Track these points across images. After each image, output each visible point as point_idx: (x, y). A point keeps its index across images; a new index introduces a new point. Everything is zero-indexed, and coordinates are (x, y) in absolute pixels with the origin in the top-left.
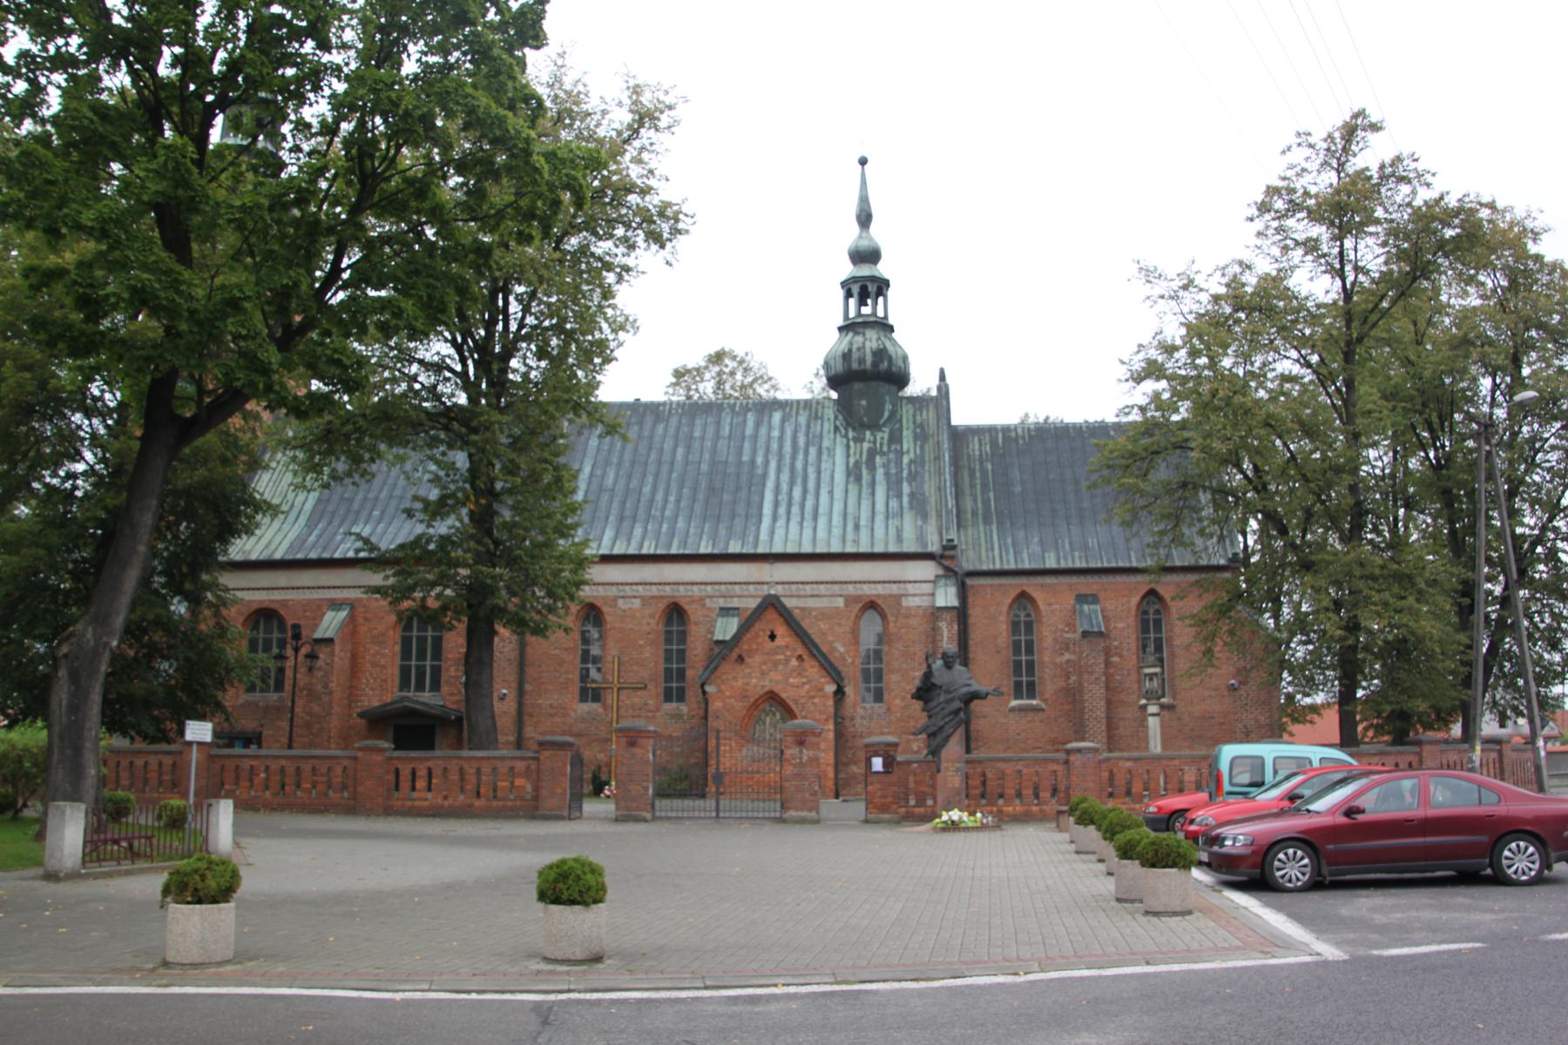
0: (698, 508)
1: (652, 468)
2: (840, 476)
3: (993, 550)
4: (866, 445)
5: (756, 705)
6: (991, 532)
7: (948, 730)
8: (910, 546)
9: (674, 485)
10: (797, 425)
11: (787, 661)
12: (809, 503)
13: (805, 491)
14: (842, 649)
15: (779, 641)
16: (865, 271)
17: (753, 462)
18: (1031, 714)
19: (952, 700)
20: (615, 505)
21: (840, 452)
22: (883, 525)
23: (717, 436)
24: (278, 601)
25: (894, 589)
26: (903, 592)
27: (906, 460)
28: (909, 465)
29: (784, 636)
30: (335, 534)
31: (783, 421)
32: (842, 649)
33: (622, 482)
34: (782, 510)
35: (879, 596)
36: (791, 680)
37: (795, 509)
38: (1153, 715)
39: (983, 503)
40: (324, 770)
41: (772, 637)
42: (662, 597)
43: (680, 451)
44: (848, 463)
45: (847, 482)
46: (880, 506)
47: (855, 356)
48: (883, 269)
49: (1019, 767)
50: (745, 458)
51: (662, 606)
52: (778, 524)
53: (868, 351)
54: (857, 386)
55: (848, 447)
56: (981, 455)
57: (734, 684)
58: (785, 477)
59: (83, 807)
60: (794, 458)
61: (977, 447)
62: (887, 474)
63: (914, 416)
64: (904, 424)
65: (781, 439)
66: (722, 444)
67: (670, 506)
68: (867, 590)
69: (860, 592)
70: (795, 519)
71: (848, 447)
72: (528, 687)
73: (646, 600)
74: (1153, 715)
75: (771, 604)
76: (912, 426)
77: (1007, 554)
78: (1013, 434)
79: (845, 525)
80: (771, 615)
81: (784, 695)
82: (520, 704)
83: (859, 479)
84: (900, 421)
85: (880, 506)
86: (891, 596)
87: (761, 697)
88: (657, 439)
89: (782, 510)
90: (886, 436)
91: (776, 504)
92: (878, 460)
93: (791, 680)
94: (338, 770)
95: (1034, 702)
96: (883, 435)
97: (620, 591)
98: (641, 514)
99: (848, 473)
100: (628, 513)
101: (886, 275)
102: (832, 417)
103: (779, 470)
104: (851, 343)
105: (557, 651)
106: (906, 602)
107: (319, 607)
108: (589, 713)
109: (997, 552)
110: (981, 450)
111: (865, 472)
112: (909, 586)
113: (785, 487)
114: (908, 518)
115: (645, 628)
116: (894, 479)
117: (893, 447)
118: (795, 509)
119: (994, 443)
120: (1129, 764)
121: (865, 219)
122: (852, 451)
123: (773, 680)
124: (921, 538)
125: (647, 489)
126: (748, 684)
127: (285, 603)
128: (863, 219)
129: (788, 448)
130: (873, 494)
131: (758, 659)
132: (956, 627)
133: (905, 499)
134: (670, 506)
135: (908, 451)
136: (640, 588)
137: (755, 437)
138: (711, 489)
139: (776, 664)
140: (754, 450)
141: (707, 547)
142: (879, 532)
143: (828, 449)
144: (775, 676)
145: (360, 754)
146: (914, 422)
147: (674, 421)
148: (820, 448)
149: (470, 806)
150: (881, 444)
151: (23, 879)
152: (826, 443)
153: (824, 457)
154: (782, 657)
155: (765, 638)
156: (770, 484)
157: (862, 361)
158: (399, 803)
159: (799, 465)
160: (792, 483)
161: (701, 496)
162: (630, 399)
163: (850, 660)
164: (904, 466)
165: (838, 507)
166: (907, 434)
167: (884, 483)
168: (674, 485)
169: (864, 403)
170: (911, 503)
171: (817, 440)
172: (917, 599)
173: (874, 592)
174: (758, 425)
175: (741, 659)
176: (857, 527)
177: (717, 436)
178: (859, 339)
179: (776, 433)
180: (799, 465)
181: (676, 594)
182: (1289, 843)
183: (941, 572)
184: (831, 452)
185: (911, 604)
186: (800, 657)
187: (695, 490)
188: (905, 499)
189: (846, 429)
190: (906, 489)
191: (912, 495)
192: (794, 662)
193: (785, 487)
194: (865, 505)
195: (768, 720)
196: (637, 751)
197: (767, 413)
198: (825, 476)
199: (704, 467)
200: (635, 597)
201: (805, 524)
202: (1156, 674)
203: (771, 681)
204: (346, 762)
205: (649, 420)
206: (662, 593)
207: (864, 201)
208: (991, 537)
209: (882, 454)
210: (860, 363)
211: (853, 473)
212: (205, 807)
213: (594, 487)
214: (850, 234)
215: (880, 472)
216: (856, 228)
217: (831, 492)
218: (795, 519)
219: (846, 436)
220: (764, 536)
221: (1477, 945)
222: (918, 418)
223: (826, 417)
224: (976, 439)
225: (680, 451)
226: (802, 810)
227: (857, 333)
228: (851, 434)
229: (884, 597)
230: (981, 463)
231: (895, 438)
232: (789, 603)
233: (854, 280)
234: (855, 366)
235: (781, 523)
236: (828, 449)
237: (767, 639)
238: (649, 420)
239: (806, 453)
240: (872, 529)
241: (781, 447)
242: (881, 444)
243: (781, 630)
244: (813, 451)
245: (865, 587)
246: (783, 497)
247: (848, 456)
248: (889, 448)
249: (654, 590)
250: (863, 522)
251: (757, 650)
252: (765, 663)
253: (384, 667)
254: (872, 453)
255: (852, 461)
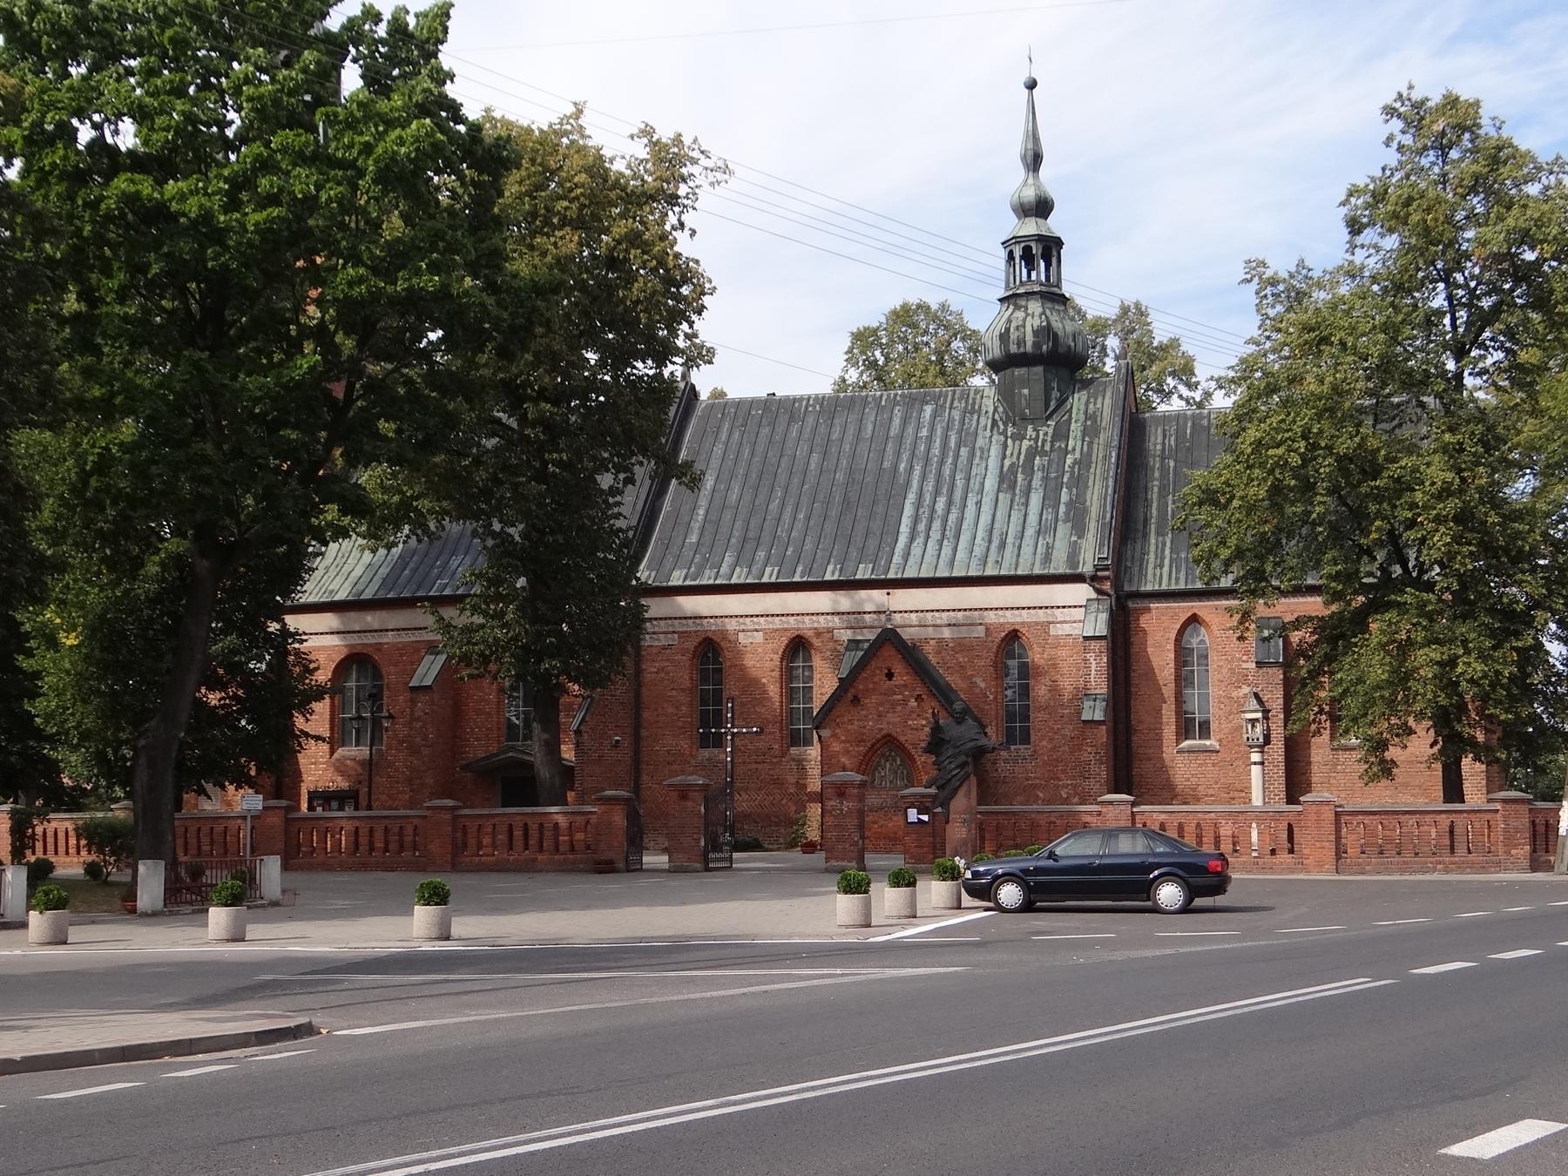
0: (829, 527)
1: (782, 478)
2: (991, 483)
3: (1161, 567)
4: (1026, 443)
5: (872, 750)
6: (1164, 544)
7: (955, 783)
8: (1059, 566)
9: (805, 500)
10: (950, 420)
11: (905, 701)
12: (952, 517)
13: (950, 503)
14: (983, 685)
15: (897, 680)
16: (1031, 227)
17: (895, 468)
18: (1202, 756)
19: (959, 754)
20: (738, 524)
21: (995, 451)
22: (1032, 542)
23: (858, 437)
24: (371, 645)
25: (1041, 616)
26: (1051, 619)
27: (1069, 461)
28: (1072, 467)
29: (902, 676)
30: (432, 566)
31: (935, 415)
32: (983, 685)
33: (747, 497)
34: (921, 527)
35: (1023, 623)
36: (910, 722)
37: (937, 525)
38: (1255, 763)
39: (1158, 509)
40: (396, 830)
41: (890, 676)
42: (786, 630)
43: (815, 457)
44: (1002, 466)
45: (999, 491)
46: (1033, 518)
47: (1014, 336)
48: (1055, 224)
49: (1053, 819)
50: (886, 464)
51: (785, 641)
52: (915, 544)
53: (1029, 329)
54: (1018, 372)
55: (1005, 446)
56: (1163, 450)
57: (850, 727)
58: (929, 487)
59: (163, 863)
60: (942, 462)
61: (1160, 439)
62: (1045, 479)
63: (1087, 404)
64: (1074, 415)
65: (930, 439)
66: (863, 447)
67: (799, 525)
68: (1011, 618)
69: (1002, 620)
70: (935, 535)
71: (1005, 446)
72: (644, 733)
73: (769, 634)
74: (1255, 763)
75: (889, 638)
76: (1082, 417)
77: (1178, 572)
78: (1205, 422)
79: (990, 541)
80: (888, 651)
81: (902, 739)
82: (637, 752)
83: (1013, 486)
84: (1070, 410)
85: (1033, 518)
86: (1037, 623)
87: (878, 741)
88: (790, 444)
89: (921, 527)
90: (1051, 431)
91: (916, 520)
92: (1037, 461)
93: (910, 722)
94: (409, 830)
95: (1208, 743)
96: (1049, 429)
97: (740, 624)
98: (766, 537)
99: (1002, 478)
100: (751, 534)
101: (1057, 232)
102: (991, 409)
103: (924, 477)
104: (1009, 321)
105: (674, 693)
106: (1058, 630)
107: (417, 650)
108: (709, 759)
109: (1166, 568)
110: (1164, 444)
111: (1020, 477)
112: (1057, 612)
113: (928, 498)
114: (1063, 530)
115: (768, 664)
116: (1053, 484)
117: (1057, 444)
118: (937, 525)
119: (1180, 434)
120: (1163, 816)
121: (1034, 161)
122: (1008, 453)
123: (891, 723)
124: (1073, 558)
125: (774, 506)
126: (865, 727)
127: (378, 647)
128: (1030, 159)
129: (936, 451)
130: (1026, 504)
131: (874, 699)
132: (1105, 659)
133: (1062, 509)
134: (799, 525)
135: (1074, 449)
136: (762, 620)
137: (901, 436)
138: (846, 500)
139: (894, 705)
140: (898, 455)
141: (833, 573)
142: (1027, 550)
143: (982, 449)
144: (893, 718)
145: (428, 813)
146: (1086, 412)
147: (810, 420)
148: (973, 448)
149: (535, 860)
150: (1044, 441)
151: (208, 1020)
152: (980, 442)
153: (977, 461)
154: (900, 697)
155: (880, 677)
156: (911, 497)
157: (1021, 342)
158: (468, 860)
159: (947, 471)
160: (937, 493)
161: (833, 513)
162: (761, 393)
163: (991, 697)
164: (1067, 469)
165: (985, 519)
166: (1076, 428)
167: (1041, 490)
168: (805, 500)
169: (1026, 391)
170: (1067, 513)
171: (970, 438)
172: (1066, 626)
173: (1018, 620)
174: (905, 422)
175: (856, 700)
176: (1003, 545)
177: (858, 437)
178: (1020, 314)
179: (924, 433)
180: (947, 471)
181: (801, 626)
182: (1014, 878)
183: (1094, 595)
184: (985, 457)
185: (1060, 633)
186: (918, 698)
187: (827, 503)
188: (1062, 509)
189: (1005, 424)
190: (1064, 497)
191: (1070, 504)
192: (913, 703)
193: (928, 498)
194: (1016, 517)
195: (888, 765)
196: (689, 804)
197: (917, 406)
198: (975, 484)
199: (840, 476)
200: (757, 631)
201: (945, 542)
202: (1257, 720)
203: (888, 723)
204: (416, 821)
205: (783, 420)
206: (785, 626)
207: (1034, 136)
208: (1163, 550)
209: (1043, 453)
210: (1019, 345)
211: (1007, 480)
212: (258, 862)
213: (717, 502)
214: (1013, 182)
215: (1038, 475)
216: (1020, 172)
217: (979, 504)
218: (935, 535)
219: (1004, 433)
220: (897, 559)
221: (1360, 983)
222: (1091, 406)
223: (984, 409)
224: (1160, 431)
225: (815, 457)
226: (843, 860)
227: (1018, 308)
228: (1010, 430)
229: (1029, 625)
230: (1163, 459)
231: (1061, 434)
232: (906, 634)
233: (1016, 240)
234: (1013, 349)
235: (920, 540)
236: (982, 449)
237: (884, 678)
238: (783, 420)
239: (957, 456)
240: (1020, 547)
241: (928, 450)
242: (1044, 441)
243: (899, 668)
244: (964, 451)
245: (1008, 613)
246: (925, 513)
247: (1004, 457)
248: (1052, 446)
249: (777, 623)
250: (1010, 540)
251: (874, 689)
252: (882, 704)
253: (489, 714)
254: (1032, 453)
255: (1007, 463)
